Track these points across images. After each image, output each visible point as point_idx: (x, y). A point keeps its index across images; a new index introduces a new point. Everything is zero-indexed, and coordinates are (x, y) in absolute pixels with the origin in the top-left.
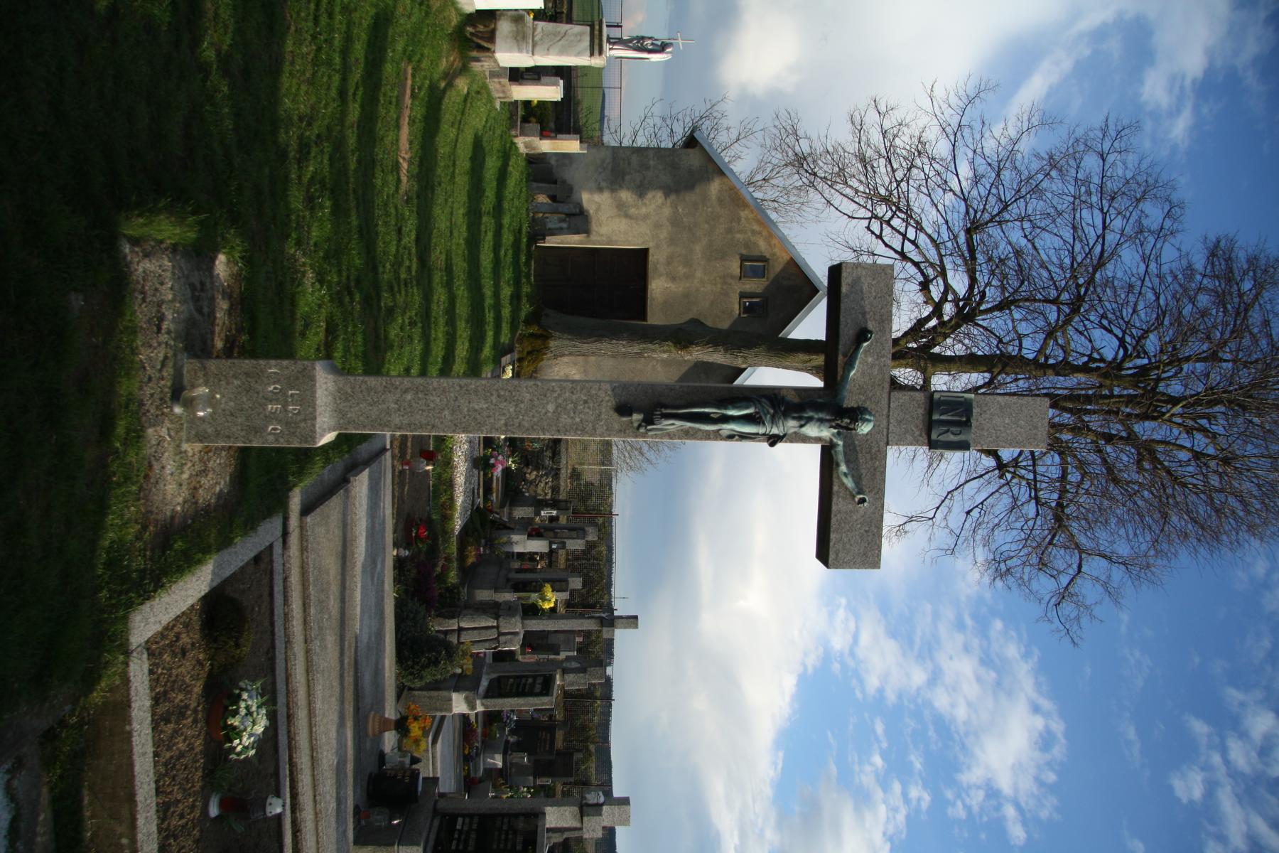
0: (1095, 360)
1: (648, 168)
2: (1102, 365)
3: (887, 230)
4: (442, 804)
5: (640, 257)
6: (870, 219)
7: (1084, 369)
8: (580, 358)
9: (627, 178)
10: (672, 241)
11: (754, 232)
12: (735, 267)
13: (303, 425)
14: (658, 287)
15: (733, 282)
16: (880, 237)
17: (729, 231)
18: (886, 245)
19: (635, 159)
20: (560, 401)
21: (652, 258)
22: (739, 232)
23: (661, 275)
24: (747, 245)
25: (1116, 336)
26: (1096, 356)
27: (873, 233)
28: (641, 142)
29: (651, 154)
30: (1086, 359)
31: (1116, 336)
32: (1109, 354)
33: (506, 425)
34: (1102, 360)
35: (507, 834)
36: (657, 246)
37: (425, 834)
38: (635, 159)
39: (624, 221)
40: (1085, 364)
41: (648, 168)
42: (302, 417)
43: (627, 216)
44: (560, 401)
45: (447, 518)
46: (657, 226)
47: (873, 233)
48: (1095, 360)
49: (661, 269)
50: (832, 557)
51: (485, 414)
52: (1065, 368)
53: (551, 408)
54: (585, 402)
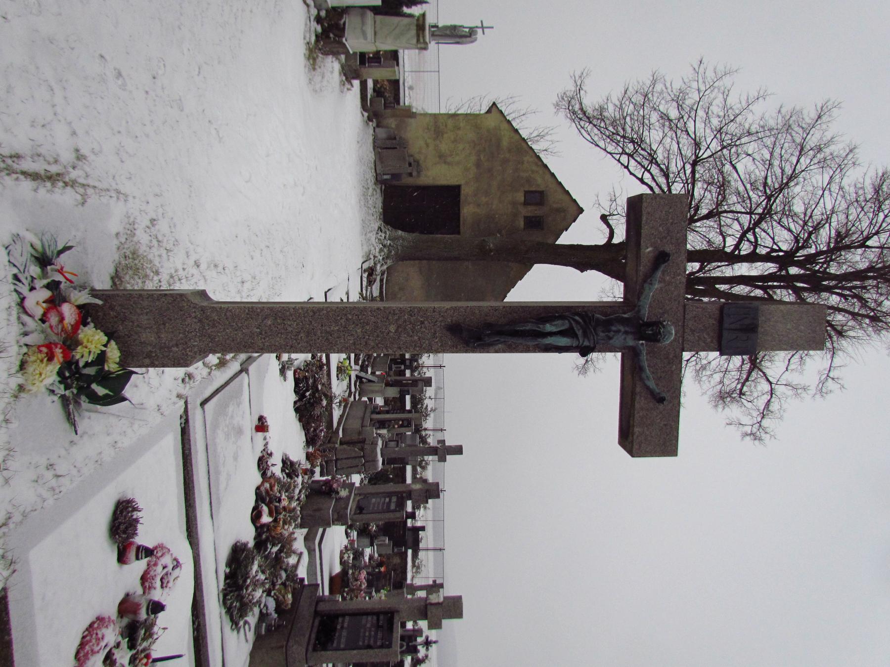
0: (776, 251)
1: (459, 129)
2: (781, 254)
3: (632, 162)
4: (322, 607)
6: (621, 154)
7: (767, 258)
8: (417, 262)
9: (445, 136)
11: (533, 171)
12: (520, 197)
13: (175, 349)
14: (467, 211)
16: (627, 167)
18: (631, 173)
19: (450, 123)
20: (400, 322)
21: (465, 191)
23: (469, 204)
24: (528, 181)
26: (775, 247)
27: (622, 164)
29: (461, 118)
30: (768, 250)
32: (785, 247)
33: (354, 344)
34: (780, 250)
35: (370, 631)
37: (307, 636)
38: (450, 123)
40: (768, 253)
41: (459, 129)
42: (174, 342)
44: (400, 322)
47: (622, 164)
48: (776, 251)
50: (636, 447)
51: (336, 335)
52: (753, 257)
53: (392, 328)
54: (422, 323)
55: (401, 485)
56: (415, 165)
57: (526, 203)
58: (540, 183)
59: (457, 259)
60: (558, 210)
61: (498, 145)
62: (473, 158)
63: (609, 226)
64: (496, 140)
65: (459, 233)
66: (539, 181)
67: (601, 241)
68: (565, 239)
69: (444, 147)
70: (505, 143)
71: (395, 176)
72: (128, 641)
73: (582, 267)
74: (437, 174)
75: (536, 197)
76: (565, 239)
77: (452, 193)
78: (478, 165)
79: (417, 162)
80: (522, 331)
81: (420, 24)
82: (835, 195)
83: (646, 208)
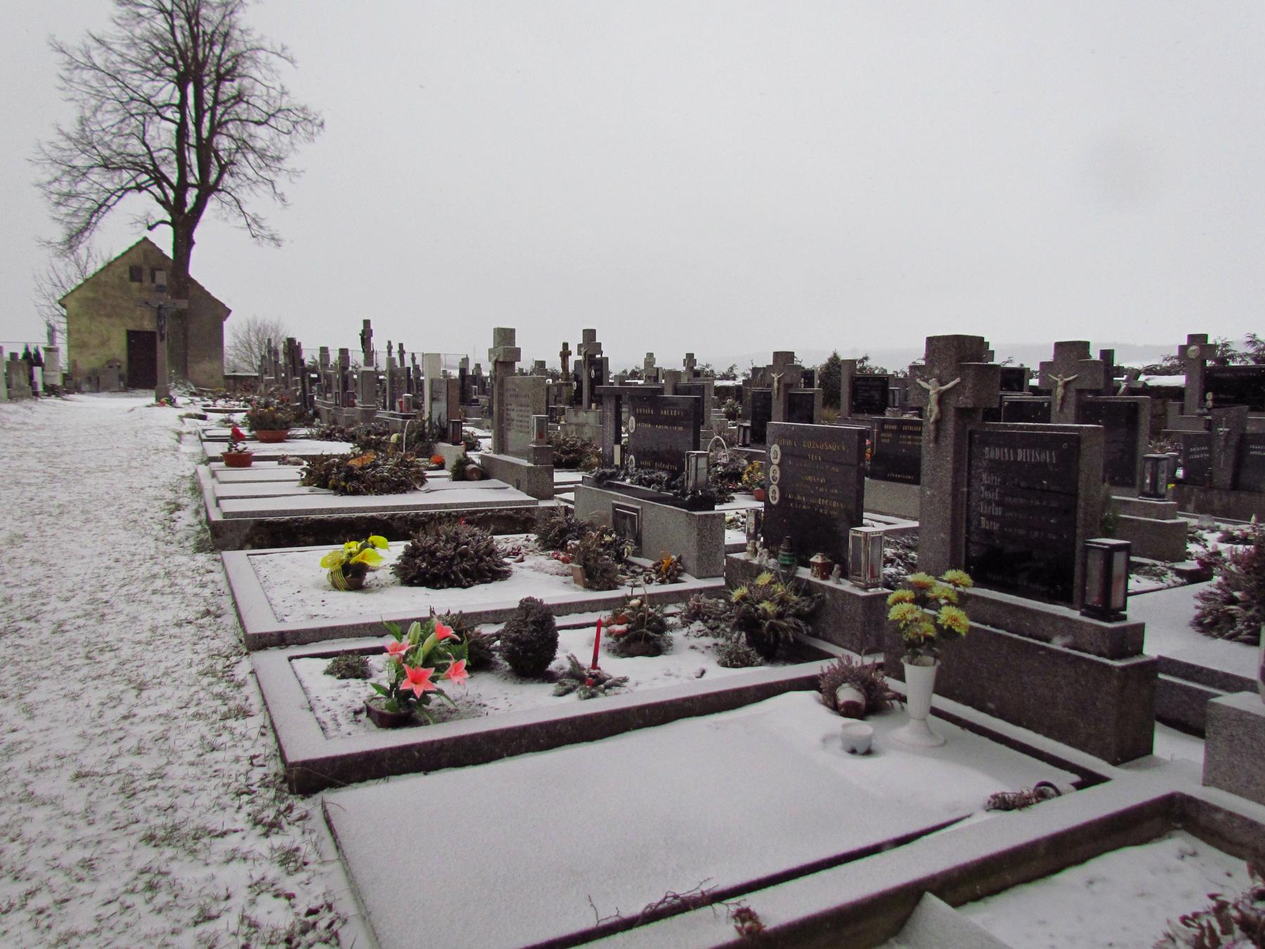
12: (135, 285)
21: (132, 327)
52: (182, 106)
55: (1236, 647)
56: (111, 364)
57: (140, 281)
58: (124, 270)
59: (186, 336)
60: (146, 256)
61: (93, 300)
62: (104, 319)
63: (158, 223)
64: (91, 299)
65: (824, 405)
66: (121, 269)
67: (170, 229)
68: (169, 252)
69: (94, 341)
70: (91, 295)
71: (121, 378)
72: (552, 658)
73: (190, 243)
74: (118, 348)
75: (135, 273)
76: (169, 252)
77: (131, 335)
78: (109, 316)
79: (108, 362)
80: (153, 360)
81: (48, 350)
82: (135, 81)
83: (238, 545)
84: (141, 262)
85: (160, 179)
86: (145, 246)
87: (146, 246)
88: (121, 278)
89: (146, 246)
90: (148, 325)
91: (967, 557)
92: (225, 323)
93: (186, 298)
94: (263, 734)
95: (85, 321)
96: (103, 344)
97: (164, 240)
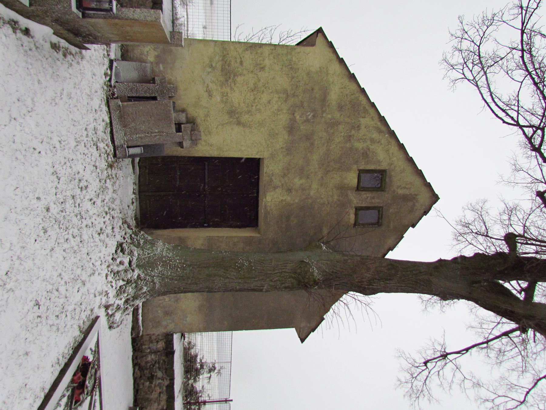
5: (253, 166)
9: (239, 79)
10: (289, 150)
11: (372, 141)
12: (352, 179)
15: (349, 193)
17: (349, 138)
21: (270, 170)
22: (359, 140)
23: (275, 188)
25: (515, 111)
28: (336, 304)
29: (266, 51)
31: (515, 111)
36: (272, 156)
39: (237, 129)
41: (262, 69)
43: (239, 123)
45: (167, 38)
46: (273, 135)
49: (276, 181)
56: (187, 125)
58: (382, 158)
60: (406, 198)
61: (324, 99)
62: (284, 118)
66: (381, 155)
69: (238, 96)
70: (334, 96)
74: (221, 140)
75: (376, 179)
78: (291, 128)
79: (191, 121)
84: (394, 192)
85: (542, 182)
86: (424, 197)
87: (422, 199)
88: (365, 154)
89: (422, 199)
90: (271, 200)
91: (518, 292)
92: (450, 259)
93: (172, 335)
94: (21, 289)
95: (282, 81)
96: (233, 114)
97: (423, 243)
